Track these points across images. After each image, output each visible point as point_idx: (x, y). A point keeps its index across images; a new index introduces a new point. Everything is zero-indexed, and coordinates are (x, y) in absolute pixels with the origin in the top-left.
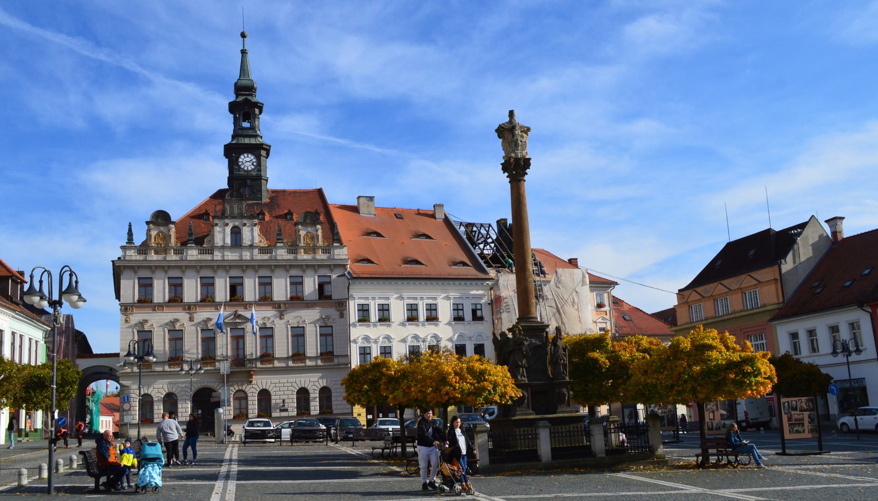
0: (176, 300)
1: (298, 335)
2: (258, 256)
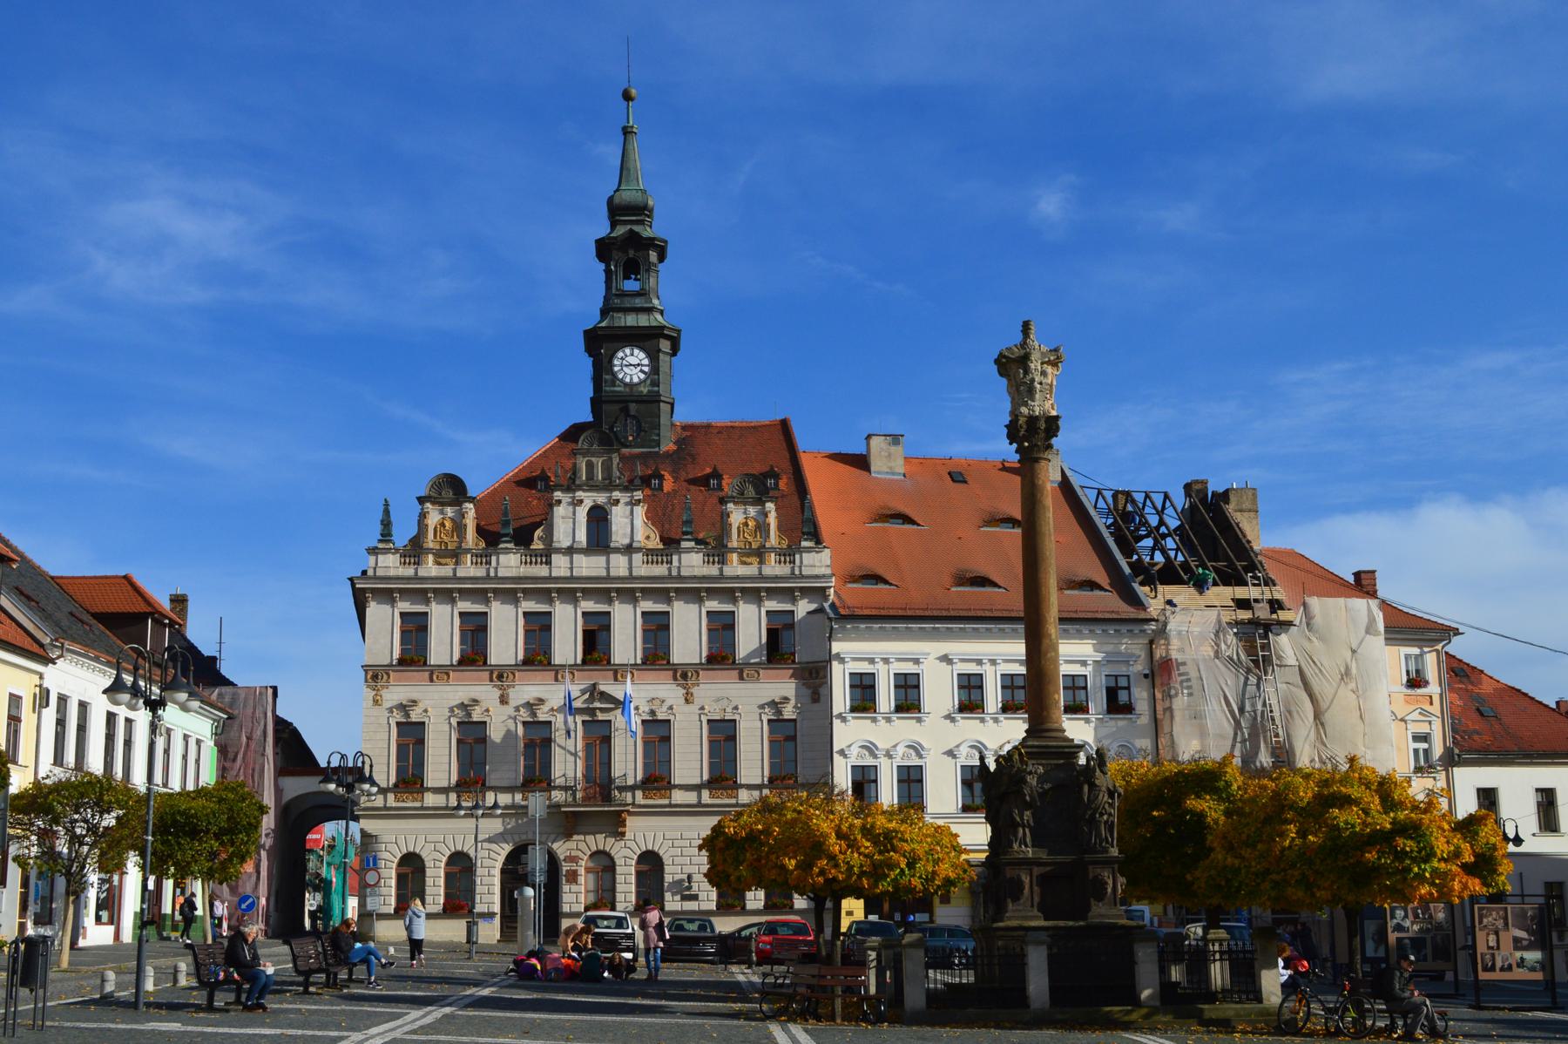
0: (474, 654)
1: (723, 735)
2: (642, 568)
